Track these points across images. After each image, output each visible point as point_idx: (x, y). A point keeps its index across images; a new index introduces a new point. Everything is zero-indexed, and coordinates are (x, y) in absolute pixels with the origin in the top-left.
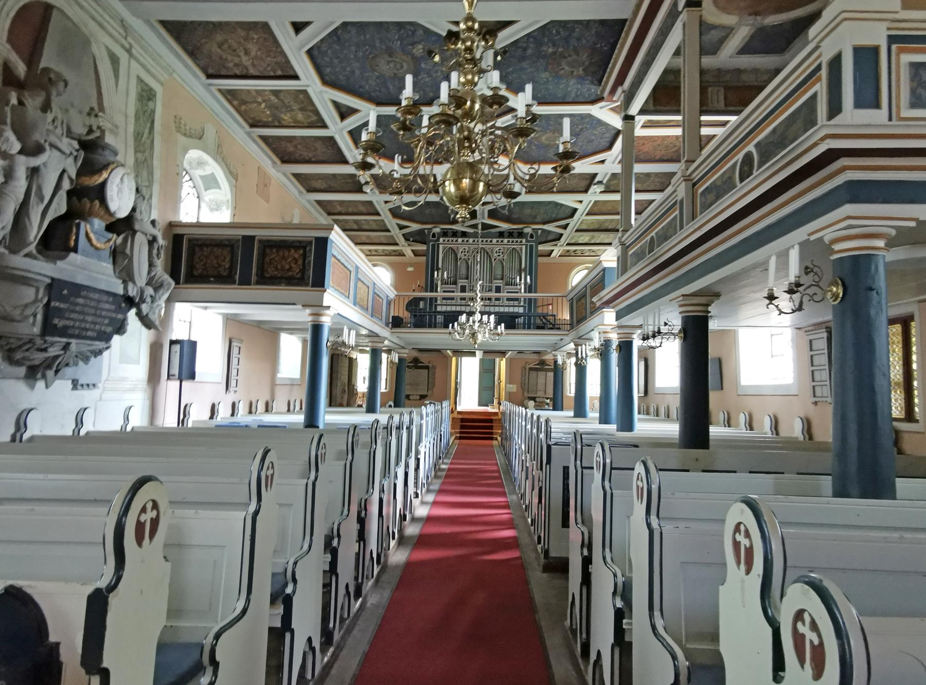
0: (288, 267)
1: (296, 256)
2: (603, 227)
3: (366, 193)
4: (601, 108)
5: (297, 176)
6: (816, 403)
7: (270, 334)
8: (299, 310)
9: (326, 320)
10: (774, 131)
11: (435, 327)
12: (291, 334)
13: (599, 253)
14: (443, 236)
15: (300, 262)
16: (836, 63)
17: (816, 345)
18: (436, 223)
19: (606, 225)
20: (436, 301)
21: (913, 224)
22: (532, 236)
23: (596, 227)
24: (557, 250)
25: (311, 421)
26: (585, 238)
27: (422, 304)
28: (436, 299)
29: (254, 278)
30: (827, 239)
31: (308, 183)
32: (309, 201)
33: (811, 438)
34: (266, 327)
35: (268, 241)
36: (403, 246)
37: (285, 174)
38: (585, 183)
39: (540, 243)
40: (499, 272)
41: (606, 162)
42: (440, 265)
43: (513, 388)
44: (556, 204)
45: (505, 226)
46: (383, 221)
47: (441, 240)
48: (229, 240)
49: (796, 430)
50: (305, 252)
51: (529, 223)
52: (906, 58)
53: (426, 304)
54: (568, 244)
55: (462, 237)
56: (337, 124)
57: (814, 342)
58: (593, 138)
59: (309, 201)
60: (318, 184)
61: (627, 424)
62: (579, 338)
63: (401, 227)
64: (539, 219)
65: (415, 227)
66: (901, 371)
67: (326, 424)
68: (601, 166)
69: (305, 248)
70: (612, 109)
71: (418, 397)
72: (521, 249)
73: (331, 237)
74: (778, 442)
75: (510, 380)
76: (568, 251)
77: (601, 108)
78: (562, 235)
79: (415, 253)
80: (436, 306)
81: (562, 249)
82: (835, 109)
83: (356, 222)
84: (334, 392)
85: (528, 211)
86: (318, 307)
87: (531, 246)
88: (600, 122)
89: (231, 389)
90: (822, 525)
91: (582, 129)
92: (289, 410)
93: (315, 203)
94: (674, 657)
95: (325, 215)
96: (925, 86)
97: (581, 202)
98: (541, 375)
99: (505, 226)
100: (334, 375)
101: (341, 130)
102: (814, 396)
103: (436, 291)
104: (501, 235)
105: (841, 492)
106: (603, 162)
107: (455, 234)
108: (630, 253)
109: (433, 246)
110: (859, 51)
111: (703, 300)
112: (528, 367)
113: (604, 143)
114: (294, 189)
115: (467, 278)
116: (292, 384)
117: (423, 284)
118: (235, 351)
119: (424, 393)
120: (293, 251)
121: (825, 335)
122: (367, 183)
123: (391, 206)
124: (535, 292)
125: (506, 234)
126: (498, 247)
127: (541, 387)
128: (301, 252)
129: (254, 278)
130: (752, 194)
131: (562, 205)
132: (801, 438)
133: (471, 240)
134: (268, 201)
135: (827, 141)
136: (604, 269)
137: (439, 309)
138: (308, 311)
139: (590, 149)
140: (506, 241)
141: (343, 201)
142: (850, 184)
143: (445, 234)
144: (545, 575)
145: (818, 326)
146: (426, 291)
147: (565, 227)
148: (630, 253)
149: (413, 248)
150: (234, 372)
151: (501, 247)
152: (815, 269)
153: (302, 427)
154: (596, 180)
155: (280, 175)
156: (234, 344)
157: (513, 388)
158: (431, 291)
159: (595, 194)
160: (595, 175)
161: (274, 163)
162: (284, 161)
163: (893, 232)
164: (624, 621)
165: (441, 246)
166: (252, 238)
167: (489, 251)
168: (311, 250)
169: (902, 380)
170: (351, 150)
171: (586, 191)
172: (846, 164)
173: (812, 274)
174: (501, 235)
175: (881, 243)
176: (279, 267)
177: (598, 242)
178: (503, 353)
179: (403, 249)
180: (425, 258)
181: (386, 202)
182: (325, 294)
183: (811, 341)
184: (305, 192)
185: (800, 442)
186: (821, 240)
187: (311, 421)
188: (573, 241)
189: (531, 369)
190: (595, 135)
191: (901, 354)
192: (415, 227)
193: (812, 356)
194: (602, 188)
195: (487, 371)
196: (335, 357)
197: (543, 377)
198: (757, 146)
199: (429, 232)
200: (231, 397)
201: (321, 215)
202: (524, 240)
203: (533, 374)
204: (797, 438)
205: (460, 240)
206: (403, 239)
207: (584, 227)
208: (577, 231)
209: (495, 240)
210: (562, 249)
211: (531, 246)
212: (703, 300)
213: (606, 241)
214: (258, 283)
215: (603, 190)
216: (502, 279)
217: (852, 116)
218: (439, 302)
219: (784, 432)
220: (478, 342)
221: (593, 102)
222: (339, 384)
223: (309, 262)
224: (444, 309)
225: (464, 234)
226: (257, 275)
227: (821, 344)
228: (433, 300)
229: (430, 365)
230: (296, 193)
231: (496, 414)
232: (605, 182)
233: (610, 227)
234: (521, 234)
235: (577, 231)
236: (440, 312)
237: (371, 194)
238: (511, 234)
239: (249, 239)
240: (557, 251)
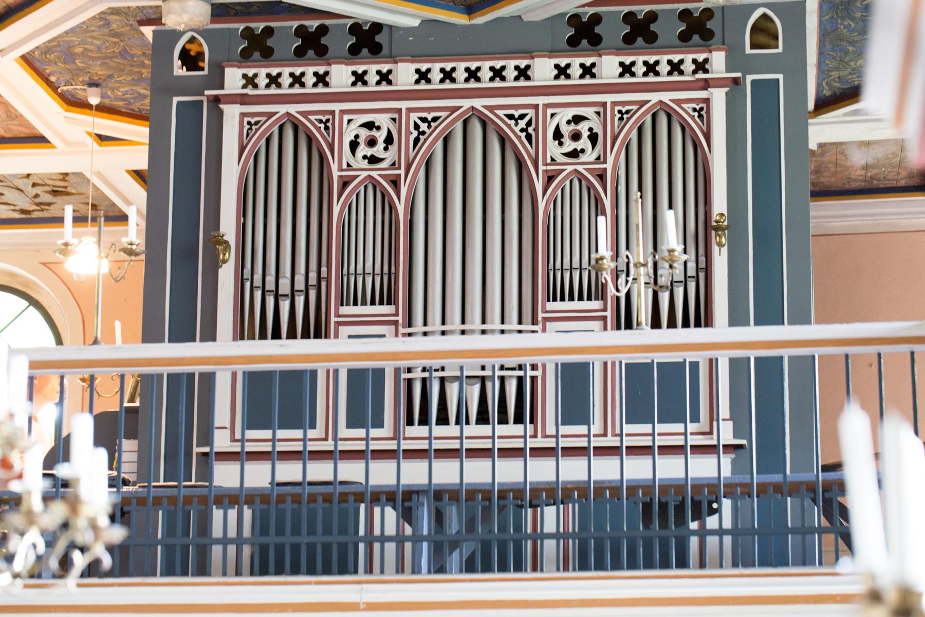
11: (203, 570)
47: (233, 79)
72: (703, 112)
103: (210, 335)
109: (190, 112)
115: (389, 298)
124: (800, 318)
133: (405, 74)
137: (225, 476)
140: (608, 67)
151: (586, 104)
165: (232, 113)
167: (514, 131)
202: (718, 61)
205: (341, 76)
209: (543, 70)
211: (765, 91)
224: (258, 476)
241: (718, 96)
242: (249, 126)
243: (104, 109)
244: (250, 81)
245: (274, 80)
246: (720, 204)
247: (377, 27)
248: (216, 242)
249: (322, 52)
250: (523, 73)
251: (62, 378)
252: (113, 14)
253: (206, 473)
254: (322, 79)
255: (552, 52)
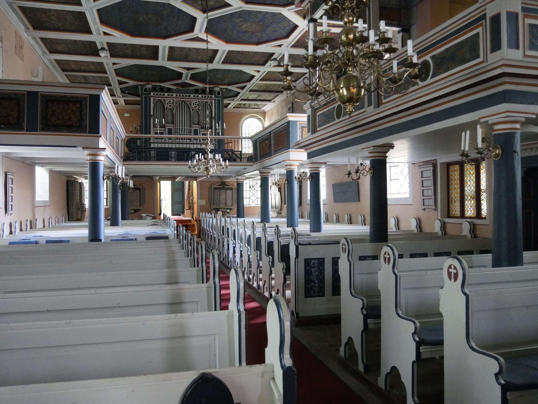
0: (68, 117)
1: (74, 109)
2: (268, 89)
3: (100, 56)
4: (289, 10)
5: (43, 40)
6: (424, 209)
7: (29, 165)
8: (80, 150)
9: (102, 159)
10: (447, 50)
11: (150, 160)
12: (42, 166)
13: (260, 106)
14: (153, 91)
15: (78, 114)
16: (496, 19)
17: (425, 174)
18: (149, 81)
19: (271, 87)
20: (150, 140)
21: (534, 116)
22: (219, 93)
23: (264, 89)
24: (233, 104)
25: (95, 236)
26: (254, 96)
27: (138, 142)
28: (150, 139)
29: (39, 126)
30: (490, 122)
31: (52, 46)
32: (49, 60)
33: (421, 231)
34: (27, 162)
35: (50, 96)
36: (119, 97)
37: (34, 38)
38: (264, 59)
39: (225, 98)
40: (196, 119)
41: (282, 46)
42: (152, 113)
43: (203, 202)
44: (241, 71)
45: (200, 85)
46: (107, 78)
47: (152, 94)
48: (15, 94)
49: (413, 226)
50: (81, 105)
51: (217, 84)
52: (529, 21)
53: (141, 143)
54: (242, 100)
55: (167, 92)
56: (90, 3)
57: (424, 173)
58: (278, 29)
59: (49, 60)
60: (60, 48)
61: (316, 227)
62: (264, 168)
63: (120, 83)
64: (226, 81)
65: (132, 83)
66: (474, 190)
67: (106, 237)
68: (279, 48)
69: (81, 103)
70: (296, 12)
71: (133, 211)
72: (212, 103)
73: (102, 94)
74: (399, 235)
75: (200, 197)
76: (240, 104)
77: (289, 10)
78: (239, 93)
79: (126, 102)
80: (150, 143)
81: (237, 103)
82: (496, 46)
83: (84, 77)
84: (71, 210)
85: (219, 76)
86: (95, 149)
87: (219, 101)
88: (285, 18)
89: (10, 212)
90: (482, 284)
91: (271, 23)
92: (44, 227)
93: (54, 62)
94: (497, 359)
95: (60, 71)
96: (537, 38)
97: (258, 71)
98: (223, 192)
99: (200, 85)
100: (70, 198)
101: (92, 8)
102: (424, 205)
103: (150, 134)
104: (197, 91)
105: (497, 263)
106: (280, 46)
107: (162, 89)
108: (318, 114)
109: (146, 98)
110: (509, 14)
111: (383, 149)
112: (213, 187)
113: (284, 33)
114: (39, 50)
115: (173, 124)
116: (44, 205)
117: (141, 127)
118: (9, 182)
119: (138, 208)
120: (71, 105)
121: (431, 168)
122: (103, 49)
123: (116, 67)
125: (200, 91)
126: (194, 100)
127: (222, 201)
128: (78, 106)
129: (39, 126)
130: (444, 90)
131: (245, 72)
132: (416, 230)
133: (174, 95)
134: (22, 60)
135: (503, 68)
136: (289, 122)
137: (152, 146)
138: (86, 152)
139: (274, 37)
140: (200, 96)
141: (78, 61)
142: (504, 92)
143: (154, 89)
144: (298, 329)
145: (426, 163)
146: (142, 133)
147: (243, 88)
148: (318, 114)
149: (125, 99)
150: (9, 199)
151: (197, 101)
152: (488, 140)
153: (87, 241)
154: (273, 58)
155: (31, 39)
156: (9, 176)
157: (203, 202)
158: (146, 133)
159: (270, 67)
160: (273, 54)
161: (27, 28)
162: (35, 28)
163: (524, 119)
164: (421, 348)
165: (152, 98)
166: (36, 93)
167: (188, 103)
168: (86, 105)
169: (474, 195)
170: (96, 24)
171: (264, 64)
172: (506, 80)
173: (486, 142)
174: (197, 91)
175: (518, 126)
176: (60, 117)
177: (262, 99)
178: (195, 178)
179: (118, 99)
180: (139, 106)
181: (114, 64)
182: (100, 139)
183: (422, 172)
184: (48, 52)
185: (415, 234)
186: (487, 122)
187: (95, 236)
188: (245, 98)
189: (215, 188)
190: (280, 27)
191: (474, 180)
192: (132, 83)
193: (422, 181)
194: (276, 63)
195: (178, 191)
196: (69, 183)
197: (224, 194)
198: (433, 57)
199: (145, 86)
200: (7, 219)
201: (57, 71)
202: (213, 96)
203: (217, 192)
204: (413, 231)
205: (166, 94)
206: (119, 92)
207: (256, 88)
208: (250, 91)
209: (192, 96)
210: (237, 103)
211: (219, 101)
212: (383, 149)
213: (268, 98)
214: (43, 130)
215: (277, 64)
216: (199, 124)
217: (507, 53)
218: (152, 141)
219: (403, 227)
220: (210, 173)
221: (284, 6)
222: (75, 204)
223: (86, 114)
224: (156, 145)
225: (169, 90)
226: (42, 123)
227: (429, 173)
228: (147, 140)
229: (141, 187)
230: (40, 52)
231: (190, 221)
232: (278, 59)
233: (273, 89)
234: (211, 92)
235: (250, 91)
236: (153, 148)
237: (105, 57)
238: (203, 91)
239: (33, 95)
240: (233, 104)
241: (213, 101)
242: (154, 100)
243: (128, 94)
244: (154, 94)
245: (157, 94)
246: (213, 115)
247: (170, 88)
248: (150, 116)
249: (163, 91)
250: (189, 96)
251: (11, 233)
252: (221, 263)
253: (150, 145)
254: (164, 95)
255: (193, 94)
